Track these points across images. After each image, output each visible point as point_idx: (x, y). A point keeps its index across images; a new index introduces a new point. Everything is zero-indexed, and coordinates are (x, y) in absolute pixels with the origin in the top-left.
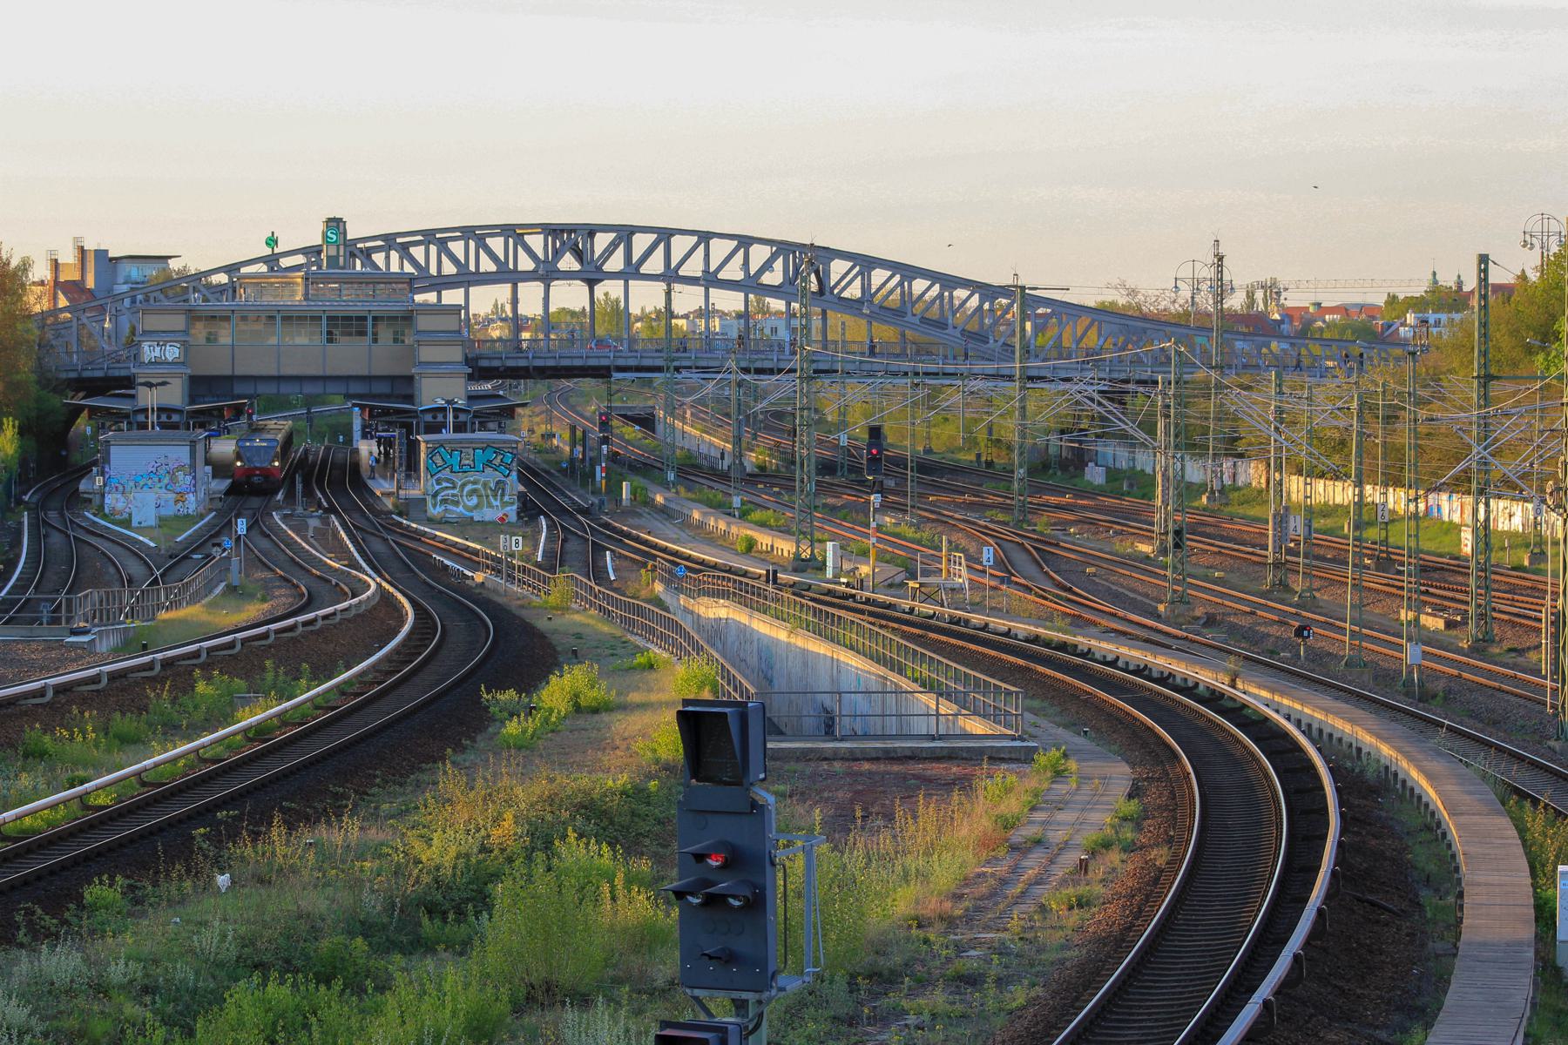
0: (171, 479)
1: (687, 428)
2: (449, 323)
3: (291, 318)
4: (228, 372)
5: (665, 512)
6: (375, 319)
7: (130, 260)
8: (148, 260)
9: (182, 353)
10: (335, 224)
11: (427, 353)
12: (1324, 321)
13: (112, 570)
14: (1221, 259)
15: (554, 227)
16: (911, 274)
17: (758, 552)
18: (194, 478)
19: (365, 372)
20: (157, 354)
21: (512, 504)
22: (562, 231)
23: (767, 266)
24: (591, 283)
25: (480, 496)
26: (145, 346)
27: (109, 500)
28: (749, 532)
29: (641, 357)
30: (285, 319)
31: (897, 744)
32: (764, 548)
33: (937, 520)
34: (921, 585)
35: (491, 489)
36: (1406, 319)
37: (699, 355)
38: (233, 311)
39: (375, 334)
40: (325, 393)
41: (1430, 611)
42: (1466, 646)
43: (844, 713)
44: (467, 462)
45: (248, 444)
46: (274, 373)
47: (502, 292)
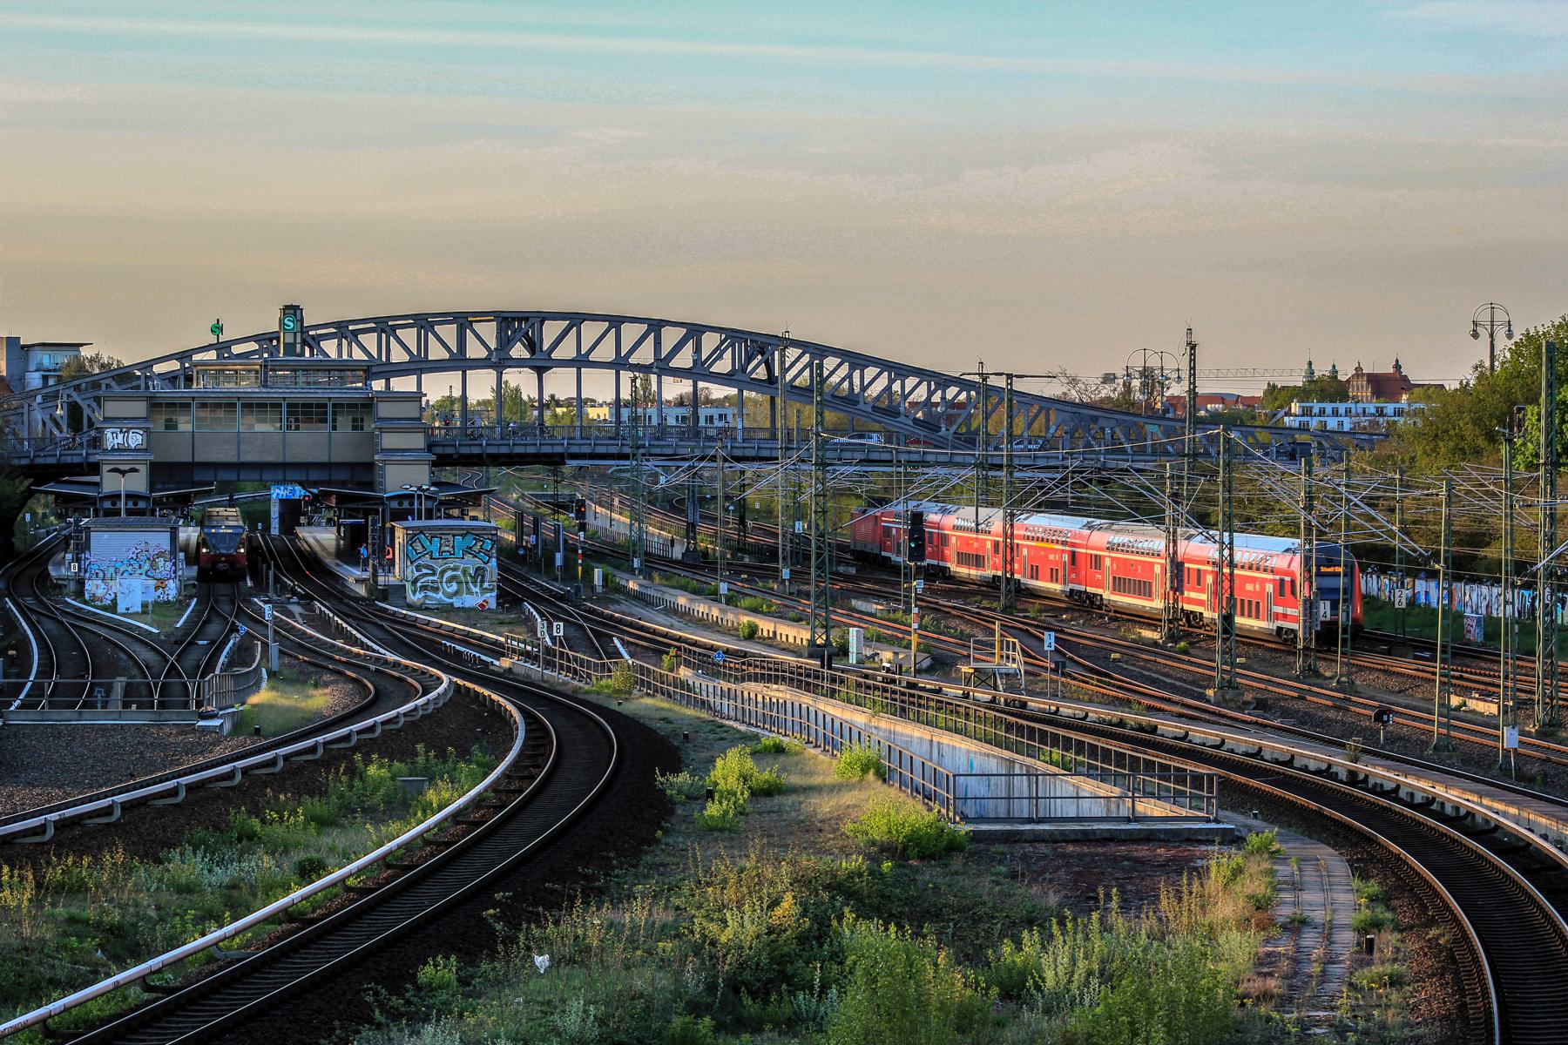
0: (152, 565)
1: (615, 516)
2: (409, 410)
3: (253, 406)
4: (189, 459)
5: (639, 598)
6: (334, 406)
7: (42, 348)
8: (60, 348)
9: (145, 440)
10: (292, 311)
11: (389, 441)
12: (1207, 410)
13: (122, 655)
14: (1193, 347)
15: (505, 315)
16: (864, 362)
17: (760, 638)
18: (175, 564)
19: (324, 458)
20: (120, 441)
21: (492, 590)
22: (514, 319)
23: (718, 353)
24: (540, 371)
25: (459, 583)
26: (108, 434)
27: (90, 586)
28: (752, 619)
29: (622, 445)
30: (244, 406)
31: (1096, 827)
32: (765, 634)
33: (927, 607)
34: (976, 670)
35: (470, 575)
36: (1290, 409)
37: (653, 443)
38: (193, 398)
39: (334, 420)
40: (238, 480)
41: (1477, 696)
42: (1533, 730)
43: (1040, 795)
44: (447, 549)
45: (213, 531)
46: (234, 459)
47: (455, 377)
